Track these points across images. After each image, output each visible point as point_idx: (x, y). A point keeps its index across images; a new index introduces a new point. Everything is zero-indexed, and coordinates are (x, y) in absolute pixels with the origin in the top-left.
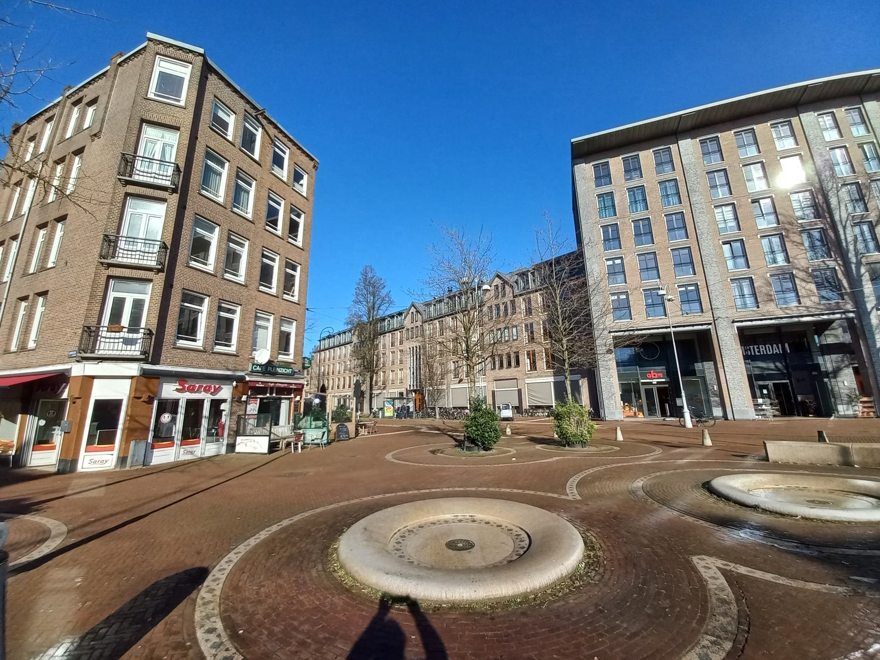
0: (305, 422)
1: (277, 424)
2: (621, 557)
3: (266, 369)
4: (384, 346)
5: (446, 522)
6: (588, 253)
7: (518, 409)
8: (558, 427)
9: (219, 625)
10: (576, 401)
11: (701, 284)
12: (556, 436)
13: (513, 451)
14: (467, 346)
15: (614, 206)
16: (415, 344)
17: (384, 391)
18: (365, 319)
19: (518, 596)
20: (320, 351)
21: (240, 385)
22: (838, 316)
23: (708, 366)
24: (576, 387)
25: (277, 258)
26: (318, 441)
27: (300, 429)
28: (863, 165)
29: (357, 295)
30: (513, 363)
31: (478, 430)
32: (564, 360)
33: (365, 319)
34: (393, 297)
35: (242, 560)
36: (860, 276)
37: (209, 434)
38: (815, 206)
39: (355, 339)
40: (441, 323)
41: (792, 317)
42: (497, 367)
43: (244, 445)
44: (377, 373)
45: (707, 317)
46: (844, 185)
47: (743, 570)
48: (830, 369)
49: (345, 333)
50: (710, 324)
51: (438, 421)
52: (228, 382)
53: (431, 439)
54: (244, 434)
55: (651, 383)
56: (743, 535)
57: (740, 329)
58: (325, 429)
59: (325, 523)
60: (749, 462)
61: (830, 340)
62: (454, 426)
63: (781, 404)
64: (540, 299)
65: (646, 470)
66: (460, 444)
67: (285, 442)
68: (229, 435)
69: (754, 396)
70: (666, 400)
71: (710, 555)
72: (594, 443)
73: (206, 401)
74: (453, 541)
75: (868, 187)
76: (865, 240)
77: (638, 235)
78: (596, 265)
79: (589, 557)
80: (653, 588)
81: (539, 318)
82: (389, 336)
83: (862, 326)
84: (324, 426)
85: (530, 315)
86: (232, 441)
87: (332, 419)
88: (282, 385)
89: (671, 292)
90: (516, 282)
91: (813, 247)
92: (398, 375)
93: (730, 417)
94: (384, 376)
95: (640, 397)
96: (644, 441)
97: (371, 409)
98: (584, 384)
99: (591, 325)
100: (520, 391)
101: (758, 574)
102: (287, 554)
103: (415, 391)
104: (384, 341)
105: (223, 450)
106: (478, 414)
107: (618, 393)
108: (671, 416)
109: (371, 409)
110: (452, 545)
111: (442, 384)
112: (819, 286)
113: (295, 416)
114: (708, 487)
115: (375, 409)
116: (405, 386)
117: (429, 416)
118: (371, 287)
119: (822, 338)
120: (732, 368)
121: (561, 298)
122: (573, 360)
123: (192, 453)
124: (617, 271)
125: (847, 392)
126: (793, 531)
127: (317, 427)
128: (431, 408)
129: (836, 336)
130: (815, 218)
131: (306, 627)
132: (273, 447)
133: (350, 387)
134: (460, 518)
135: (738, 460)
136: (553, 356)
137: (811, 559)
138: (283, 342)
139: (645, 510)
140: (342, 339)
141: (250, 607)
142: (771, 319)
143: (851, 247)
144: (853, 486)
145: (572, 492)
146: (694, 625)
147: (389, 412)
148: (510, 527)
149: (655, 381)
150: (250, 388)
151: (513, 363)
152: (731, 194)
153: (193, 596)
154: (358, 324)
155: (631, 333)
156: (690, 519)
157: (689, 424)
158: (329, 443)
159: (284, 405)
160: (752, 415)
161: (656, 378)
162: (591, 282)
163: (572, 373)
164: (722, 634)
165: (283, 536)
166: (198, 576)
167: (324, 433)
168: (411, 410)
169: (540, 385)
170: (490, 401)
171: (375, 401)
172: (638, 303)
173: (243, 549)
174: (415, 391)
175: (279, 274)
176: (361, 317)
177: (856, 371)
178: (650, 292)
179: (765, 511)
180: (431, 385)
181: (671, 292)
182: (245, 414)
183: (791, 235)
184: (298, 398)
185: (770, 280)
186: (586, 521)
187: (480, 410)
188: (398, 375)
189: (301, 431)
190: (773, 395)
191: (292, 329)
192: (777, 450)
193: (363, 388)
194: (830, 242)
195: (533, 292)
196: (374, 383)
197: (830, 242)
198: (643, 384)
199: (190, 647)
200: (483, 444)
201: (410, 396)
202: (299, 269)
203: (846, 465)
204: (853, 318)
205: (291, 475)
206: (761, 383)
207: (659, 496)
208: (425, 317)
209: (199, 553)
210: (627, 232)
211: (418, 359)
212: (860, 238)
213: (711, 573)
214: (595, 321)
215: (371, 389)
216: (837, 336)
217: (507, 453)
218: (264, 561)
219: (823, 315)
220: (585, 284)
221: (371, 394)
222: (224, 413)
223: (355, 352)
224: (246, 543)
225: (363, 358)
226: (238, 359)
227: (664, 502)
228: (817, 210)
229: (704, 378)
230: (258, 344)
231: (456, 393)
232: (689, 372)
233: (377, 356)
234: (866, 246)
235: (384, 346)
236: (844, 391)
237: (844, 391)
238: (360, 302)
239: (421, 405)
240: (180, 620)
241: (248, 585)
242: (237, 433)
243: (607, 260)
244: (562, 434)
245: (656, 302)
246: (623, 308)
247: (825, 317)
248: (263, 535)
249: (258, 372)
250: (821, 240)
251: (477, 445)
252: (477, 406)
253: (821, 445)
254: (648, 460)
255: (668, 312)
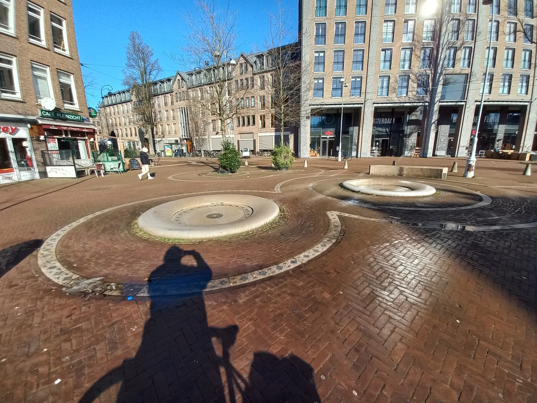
0: (103, 157)
1: (79, 157)
2: (296, 214)
3: (55, 114)
4: (159, 105)
5: (207, 206)
6: (304, 43)
7: (253, 152)
8: (274, 159)
9: (58, 264)
10: (286, 145)
11: (364, 77)
12: (273, 165)
13: (248, 173)
14: (220, 106)
15: (326, 7)
16: (182, 104)
17: (164, 139)
18: (139, 81)
19: (244, 233)
20: (105, 107)
21: (34, 127)
22: (421, 104)
23: (356, 128)
24: (286, 139)
25: (42, 11)
26: (117, 170)
27: (99, 161)
28: (466, 8)
29: (129, 59)
30: (251, 123)
31: (228, 161)
32: (281, 120)
33: (139, 81)
34: (161, 64)
35: (69, 233)
36: (439, 81)
37: (20, 165)
38: (434, 32)
39: (134, 98)
40: (201, 91)
41: (401, 103)
42: (241, 125)
43: (53, 172)
44: (156, 126)
45: (362, 100)
46: (453, 19)
47: (346, 215)
48: (408, 133)
49: (124, 92)
50: (362, 104)
51: (203, 158)
52: (23, 125)
53: (198, 168)
54: (51, 165)
55: (326, 138)
56: (351, 203)
57: (376, 108)
58: (120, 162)
59: (127, 211)
60: (361, 175)
61: (414, 118)
62: (213, 161)
63: (382, 150)
64: (270, 77)
65: (314, 179)
66: (216, 170)
67: (89, 170)
68: (38, 165)
69: (372, 146)
70: (331, 148)
71: (335, 211)
72: (292, 168)
73: (7, 140)
74: (211, 215)
75: (464, 24)
76: (449, 59)
77: (337, 35)
78: (308, 55)
79: (281, 215)
80: (308, 224)
81: (269, 92)
82: (162, 98)
83: (430, 110)
84: (119, 159)
85: (262, 92)
86: (42, 170)
87: (125, 157)
88: (75, 129)
89: (348, 81)
90: (255, 62)
91: (424, 60)
92: (172, 128)
93: (359, 156)
94: (162, 129)
95: (319, 146)
96: (317, 167)
97: (155, 151)
98: (292, 138)
99: (300, 97)
100: (254, 141)
101: (353, 216)
102: (102, 228)
103: (186, 139)
104: (158, 101)
105: (37, 176)
106: (227, 152)
107: (309, 142)
108: (333, 156)
109: (155, 151)
110: (210, 216)
111: (204, 135)
112: (419, 86)
113: (93, 153)
114: (342, 186)
115: (158, 151)
116: (178, 136)
117: (197, 156)
118: (140, 54)
119: (411, 116)
120: (366, 130)
121: (283, 75)
122: (287, 119)
123: (9, 178)
124: (320, 62)
125: (411, 145)
126: (370, 200)
127: (113, 161)
128: (198, 151)
129: (416, 116)
130: (431, 40)
131: (120, 258)
132: (80, 173)
133: (136, 135)
134: (215, 204)
135: (357, 174)
136: (276, 117)
137: (375, 210)
138: (65, 92)
139: (311, 195)
140: (123, 97)
141: (79, 254)
142: (391, 103)
143: (441, 63)
144: (400, 183)
145: (277, 190)
146: (322, 235)
147: (169, 153)
148: (243, 206)
149: (328, 137)
150: (46, 130)
151: (251, 123)
152: (395, 13)
153: (34, 253)
154: (134, 86)
155: (321, 106)
156: (330, 198)
157: (340, 160)
158: (125, 171)
159: (81, 145)
160: (368, 155)
161: (329, 135)
162: (303, 65)
163: (285, 130)
164: (333, 237)
165: (97, 220)
166: (37, 244)
167: (119, 164)
168: (184, 151)
169: (266, 137)
170: (236, 144)
171: (157, 146)
172: (328, 87)
173: (67, 228)
174: (186, 139)
175: (46, 27)
176: (135, 79)
177: (419, 135)
178: (336, 79)
179: (362, 193)
180: (197, 135)
181: (348, 81)
182: (47, 150)
183: (416, 50)
184: (92, 140)
185: (398, 79)
186: (281, 201)
187: (228, 149)
188: (172, 128)
189: (101, 163)
190: (380, 146)
191: (71, 81)
192: (374, 169)
193: (146, 136)
194: (433, 60)
195: (266, 72)
196: (155, 133)
197: (433, 60)
198: (323, 138)
199: (39, 277)
200: (231, 169)
201: (183, 142)
202: (64, 22)
203: (400, 175)
204: (427, 106)
205: (98, 189)
206: (377, 139)
207: (318, 190)
208: (189, 85)
209: (32, 233)
210: (331, 31)
211: (187, 116)
212: (447, 57)
213: (333, 217)
214: (302, 102)
215: (153, 137)
216: (417, 116)
217: (243, 173)
218: (85, 233)
219: (415, 103)
220: (299, 66)
221: (154, 141)
222: (27, 149)
223: (136, 109)
224: (70, 225)
225: (143, 114)
226: (25, 105)
227: (320, 192)
228: (434, 35)
229: (352, 135)
230: (41, 93)
231: (213, 142)
232: (346, 132)
233: (155, 113)
234: (448, 64)
235: (159, 105)
236: (410, 144)
237: (410, 144)
238: (133, 66)
239: (191, 148)
240: (28, 265)
241: (75, 244)
242: (45, 164)
243: (316, 52)
244: (276, 164)
245: (338, 88)
246: (320, 89)
247: (415, 104)
248: (82, 220)
249: (47, 117)
250: (429, 57)
251: (227, 170)
252: (227, 146)
253: (393, 166)
254: (317, 175)
255: (343, 95)
